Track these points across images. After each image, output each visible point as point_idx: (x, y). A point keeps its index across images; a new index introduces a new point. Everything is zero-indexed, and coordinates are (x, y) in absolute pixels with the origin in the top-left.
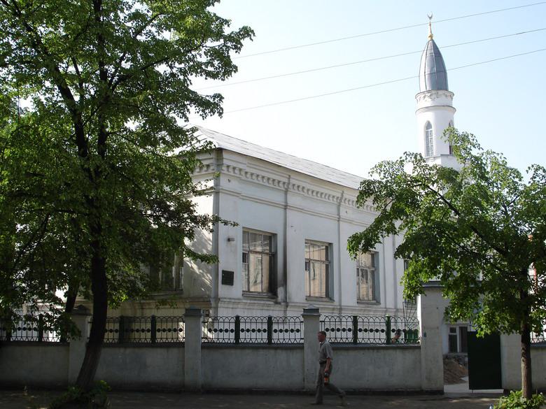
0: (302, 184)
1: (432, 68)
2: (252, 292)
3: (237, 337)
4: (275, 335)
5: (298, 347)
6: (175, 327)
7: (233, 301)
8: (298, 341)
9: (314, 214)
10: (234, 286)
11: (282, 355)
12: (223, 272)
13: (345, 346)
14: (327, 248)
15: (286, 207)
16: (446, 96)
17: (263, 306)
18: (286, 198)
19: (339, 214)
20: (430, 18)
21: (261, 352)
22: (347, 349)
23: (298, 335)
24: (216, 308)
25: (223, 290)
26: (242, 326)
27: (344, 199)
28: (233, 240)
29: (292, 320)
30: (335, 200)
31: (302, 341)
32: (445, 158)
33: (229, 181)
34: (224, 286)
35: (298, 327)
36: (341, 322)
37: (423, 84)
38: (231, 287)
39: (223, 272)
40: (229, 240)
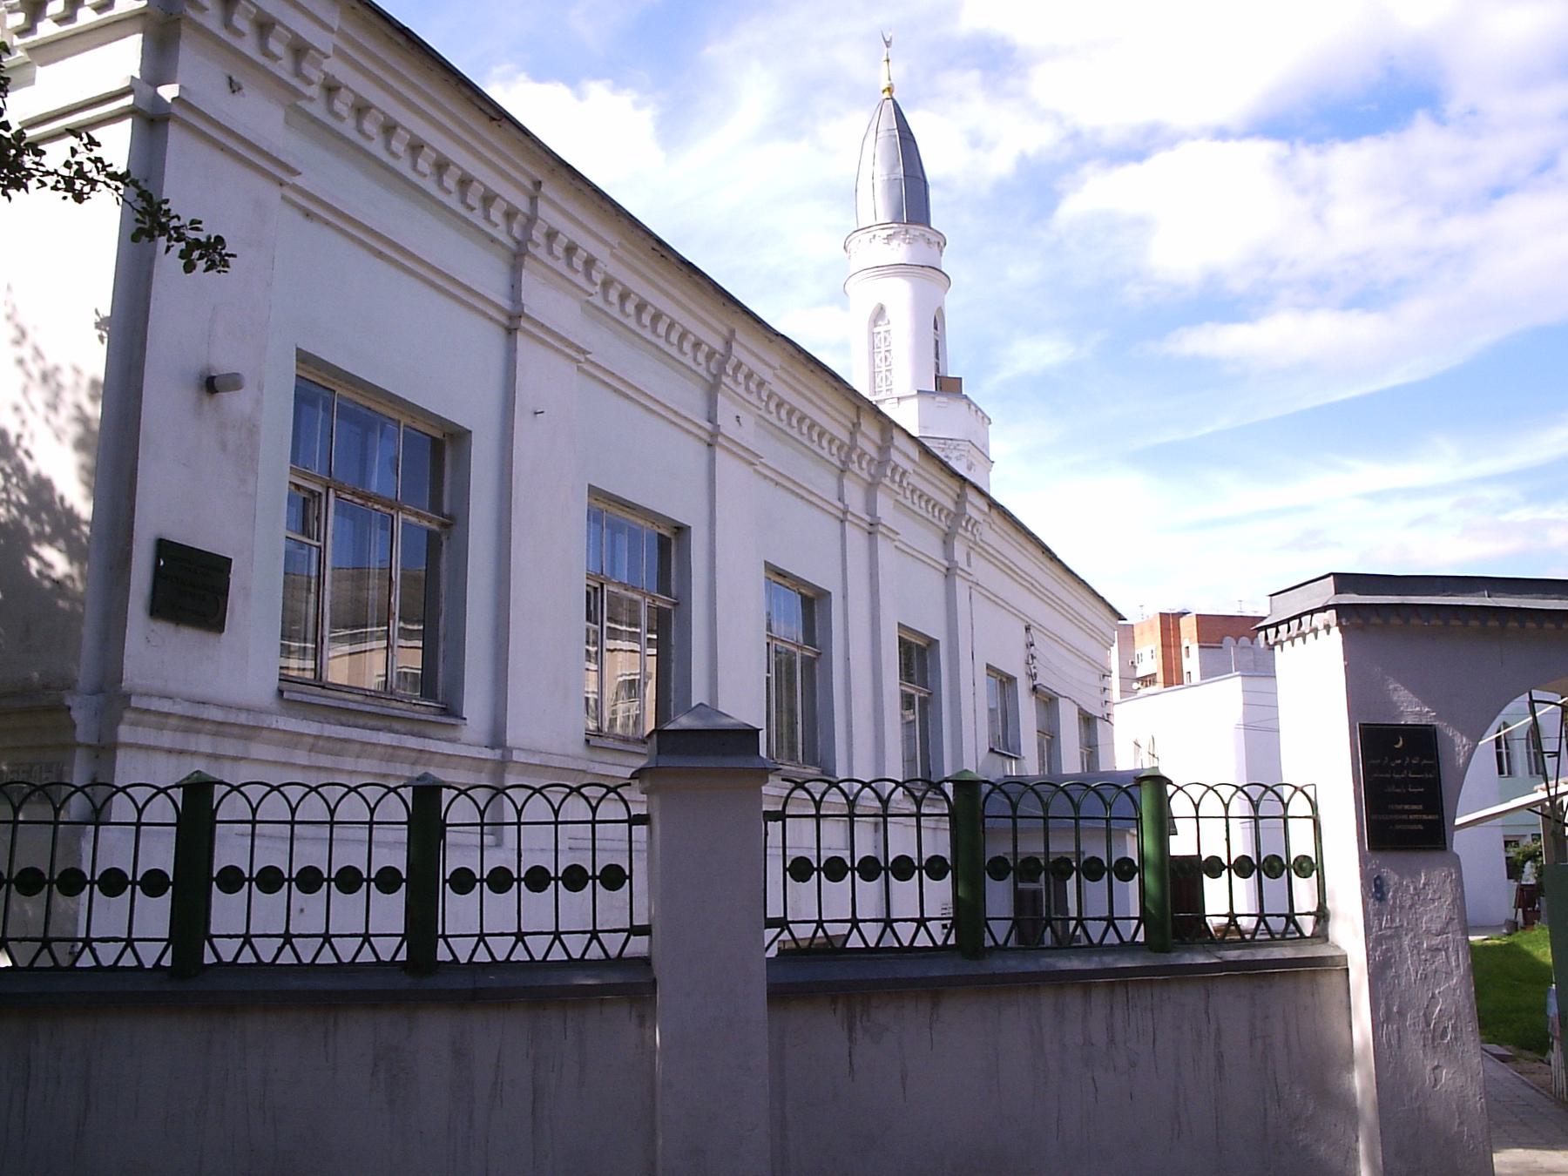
0: (588, 245)
1: (892, 168)
2: (338, 688)
3: (190, 925)
4: (458, 912)
5: (627, 983)
6: (1094, 849)
7: (217, 714)
8: (613, 944)
9: (626, 391)
10: (153, 538)
11: (499, 1039)
12: (164, 548)
13: (906, 970)
14: (664, 544)
15: (513, 323)
16: (929, 242)
17: (390, 759)
18: (515, 288)
19: (712, 419)
20: (888, 44)
21: (358, 1034)
22: (934, 990)
23: (612, 907)
24: (105, 750)
25: (156, 654)
26: (229, 850)
27: (733, 361)
28: (234, 382)
29: (538, 809)
30: (701, 358)
31: (639, 946)
32: (927, 401)
33: (234, 87)
34: (163, 629)
35: (613, 846)
36: (1014, 818)
37: (876, 203)
38: (209, 637)
39: (164, 548)
40: (211, 385)
